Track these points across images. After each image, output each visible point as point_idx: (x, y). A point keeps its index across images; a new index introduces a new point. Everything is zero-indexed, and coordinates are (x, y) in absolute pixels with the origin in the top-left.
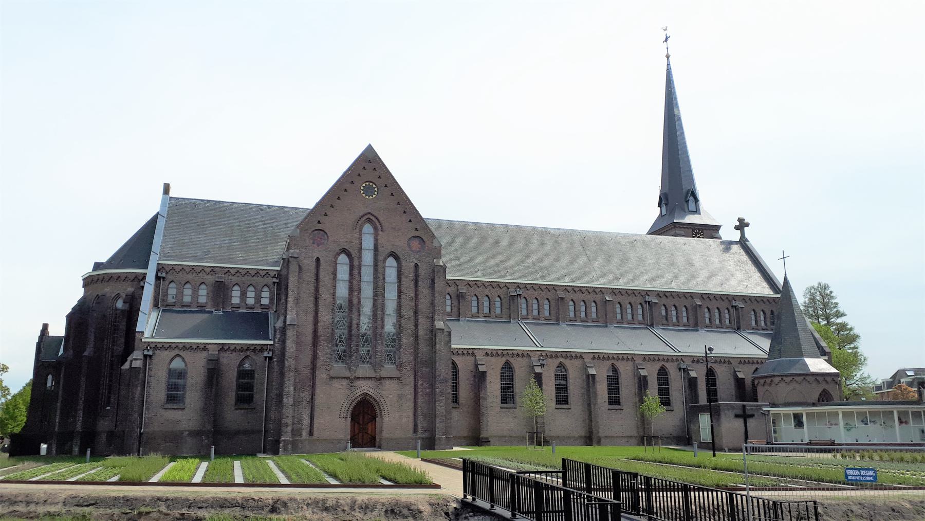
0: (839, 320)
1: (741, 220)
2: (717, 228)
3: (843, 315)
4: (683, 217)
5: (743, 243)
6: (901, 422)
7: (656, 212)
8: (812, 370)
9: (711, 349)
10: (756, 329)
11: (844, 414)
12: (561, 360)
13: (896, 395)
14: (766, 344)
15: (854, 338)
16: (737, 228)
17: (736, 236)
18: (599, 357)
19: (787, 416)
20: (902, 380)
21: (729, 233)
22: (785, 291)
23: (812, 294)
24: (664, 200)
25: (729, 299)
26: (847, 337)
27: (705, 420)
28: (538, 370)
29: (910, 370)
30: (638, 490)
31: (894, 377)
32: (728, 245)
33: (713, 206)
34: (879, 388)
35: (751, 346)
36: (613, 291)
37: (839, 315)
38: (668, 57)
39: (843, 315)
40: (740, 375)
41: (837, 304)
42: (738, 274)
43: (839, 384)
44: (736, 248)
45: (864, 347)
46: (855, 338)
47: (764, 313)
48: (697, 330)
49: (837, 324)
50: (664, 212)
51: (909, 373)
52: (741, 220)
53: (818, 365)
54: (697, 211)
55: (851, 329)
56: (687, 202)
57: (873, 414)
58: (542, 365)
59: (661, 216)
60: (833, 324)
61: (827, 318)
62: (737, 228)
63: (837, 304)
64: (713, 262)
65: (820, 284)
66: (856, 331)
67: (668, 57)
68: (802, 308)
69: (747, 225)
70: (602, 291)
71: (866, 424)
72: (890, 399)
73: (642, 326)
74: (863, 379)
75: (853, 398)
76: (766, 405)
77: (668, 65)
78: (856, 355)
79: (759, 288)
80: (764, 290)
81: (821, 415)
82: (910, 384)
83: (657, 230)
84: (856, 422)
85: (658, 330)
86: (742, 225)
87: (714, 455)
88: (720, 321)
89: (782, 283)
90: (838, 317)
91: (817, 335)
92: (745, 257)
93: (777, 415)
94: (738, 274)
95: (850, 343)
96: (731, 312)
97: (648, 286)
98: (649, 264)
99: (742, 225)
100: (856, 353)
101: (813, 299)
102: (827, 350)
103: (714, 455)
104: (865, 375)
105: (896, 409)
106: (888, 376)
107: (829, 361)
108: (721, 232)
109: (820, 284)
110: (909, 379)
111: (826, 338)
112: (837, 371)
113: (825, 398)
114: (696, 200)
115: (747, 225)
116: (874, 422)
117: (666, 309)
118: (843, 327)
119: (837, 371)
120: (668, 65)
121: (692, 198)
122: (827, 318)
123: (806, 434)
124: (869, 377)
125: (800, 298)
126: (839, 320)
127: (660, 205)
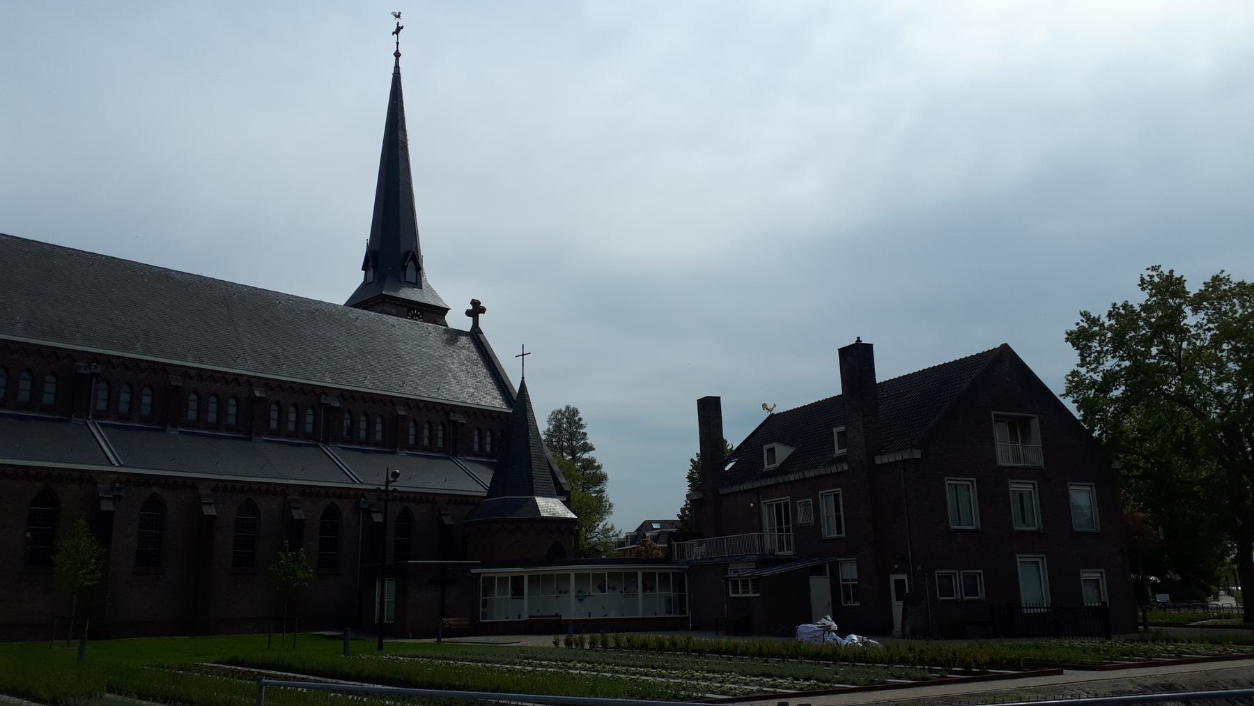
0: (586, 456)
1: (475, 303)
2: (444, 311)
3: (592, 449)
4: (397, 290)
5: (475, 335)
6: (645, 589)
7: (358, 277)
8: (544, 514)
9: (395, 475)
10: (479, 455)
11: (581, 577)
12: (156, 489)
13: (639, 552)
14: (486, 476)
15: (602, 478)
16: (469, 313)
17: (466, 324)
18: (223, 488)
19: (503, 581)
20: (647, 534)
21: (458, 320)
22: (519, 401)
23: (558, 421)
24: (372, 261)
25: (446, 411)
26: (594, 476)
27: (388, 590)
28: (106, 506)
29: (656, 522)
30: (1004, 474)
31: (639, 530)
32: (455, 335)
33: (446, 282)
34: (621, 543)
35: (469, 479)
36: (268, 384)
37: (587, 448)
38: (397, 55)
39: (592, 449)
40: (448, 521)
41: (585, 434)
42: (463, 377)
43: (577, 535)
44: (464, 340)
45: (611, 491)
46: (604, 477)
47: (492, 435)
48: (394, 453)
49: (584, 460)
50: (370, 279)
51: (655, 526)
52: (475, 303)
53: (550, 506)
54: (418, 283)
55: (599, 467)
56: (405, 268)
57: (612, 576)
58: (117, 499)
59: (365, 284)
60: (579, 459)
61: (573, 453)
62: (469, 313)
63: (585, 434)
64: (430, 357)
65: (568, 408)
66: (604, 470)
67: (397, 55)
68: (543, 437)
69: (483, 310)
70: (250, 381)
71: (604, 591)
72: (633, 556)
73: (311, 442)
74: (605, 531)
75: (593, 554)
76: (476, 566)
77: (397, 67)
78: (600, 499)
79: (489, 398)
80: (493, 401)
81: (548, 579)
82: (655, 539)
83: (358, 301)
84: (591, 589)
85: (329, 450)
86: (476, 310)
87: (380, 647)
88: (430, 441)
89: (517, 388)
90: (585, 451)
91: (556, 468)
92: (475, 355)
93: (490, 581)
94: (463, 377)
95: (596, 485)
96: (451, 429)
97: (328, 382)
98: (335, 347)
99: (476, 310)
100: (602, 497)
101: (558, 427)
102: (567, 488)
103: (380, 647)
104: (609, 526)
105: (640, 569)
106: (633, 528)
107: (567, 504)
108: (448, 318)
109: (568, 408)
110: (654, 533)
111: (569, 477)
112: (574, 516)
113: (557, 555)
114: (418, 268)
115: (483, 310)
116: (614, 589)
117: (352, 418)
118: (590, 463)
119: (574, 516)
120: (397, 67)
121: (411, 263)
122: (573, 453)
123: (525, 609)
124: (612, 528)
125: (543, 425)
126: (586, 456)
127: (365, 268)
